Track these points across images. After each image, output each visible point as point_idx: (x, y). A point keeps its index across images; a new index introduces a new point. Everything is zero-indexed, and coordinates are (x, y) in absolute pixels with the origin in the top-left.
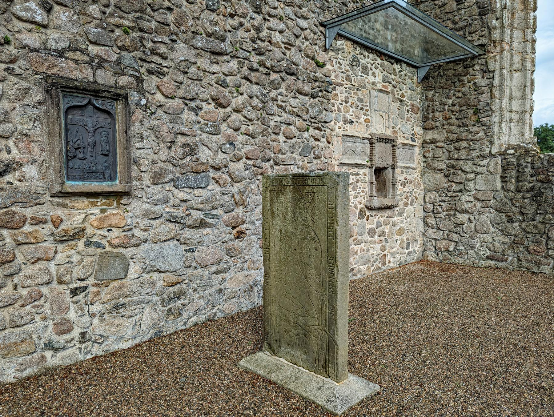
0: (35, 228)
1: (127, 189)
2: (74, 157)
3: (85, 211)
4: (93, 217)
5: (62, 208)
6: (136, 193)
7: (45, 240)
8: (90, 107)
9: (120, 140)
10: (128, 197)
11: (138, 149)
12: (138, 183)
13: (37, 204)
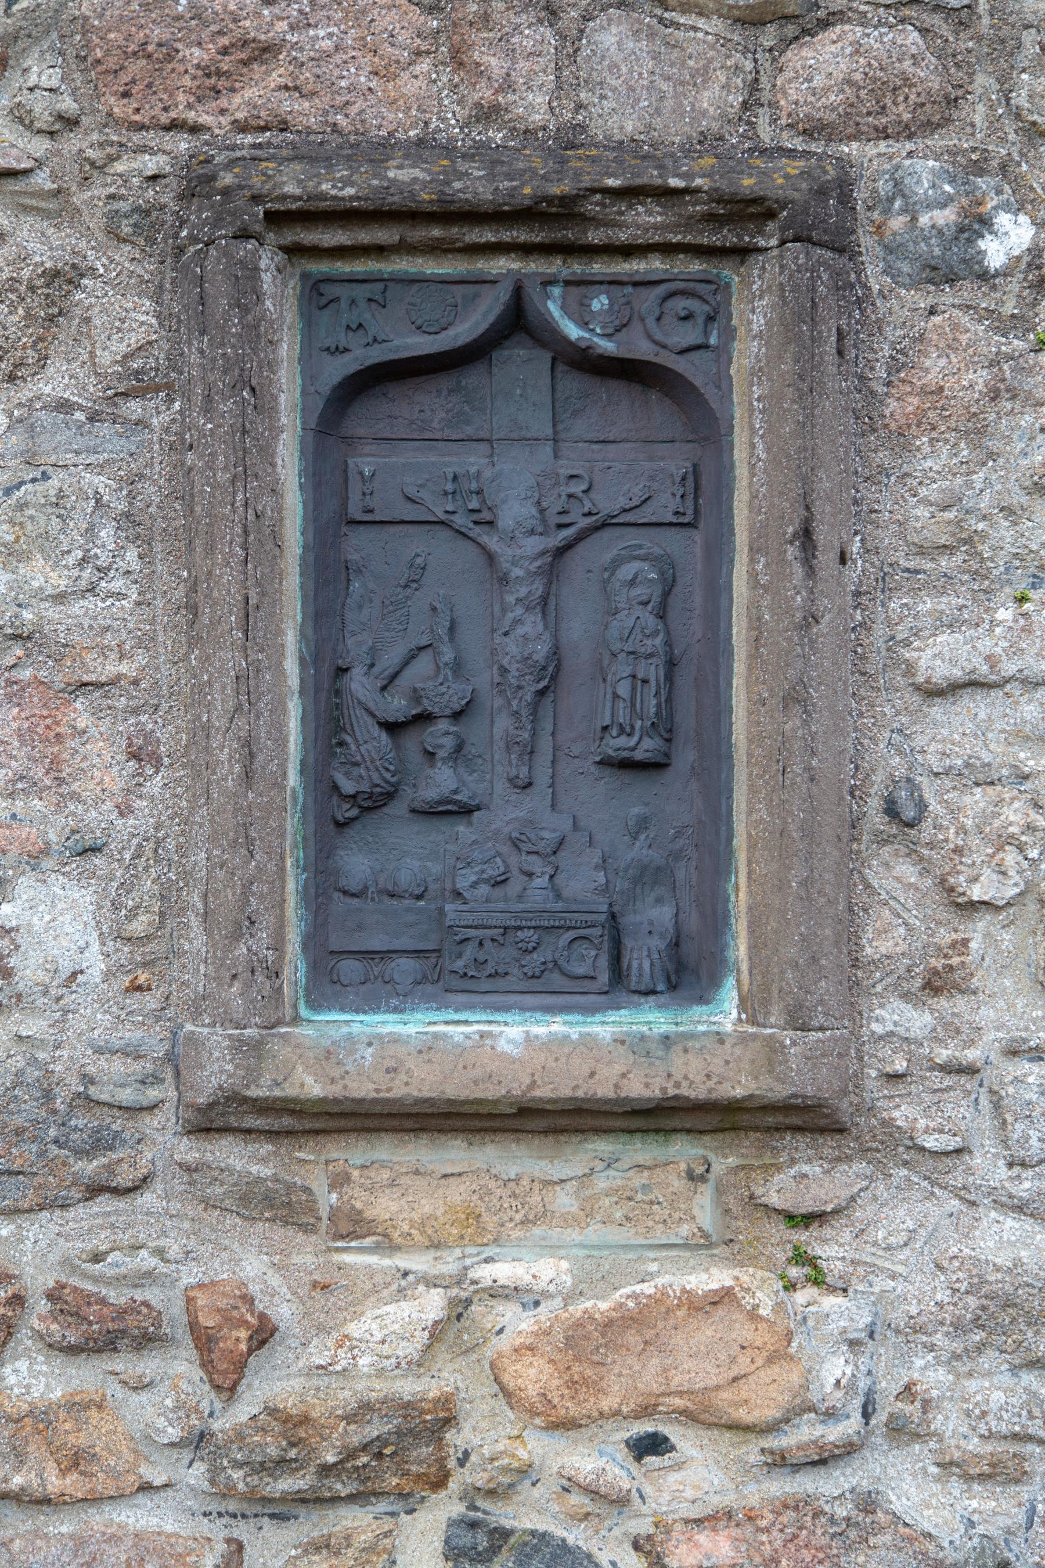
0: (86, 1376)
1: (798, 1078)
2: (374, 802)
3: (449, 1264)
4: (518, 1322)
5: (278, 1233)
6: (902, 1114)
7: (146, 1488)
8: (522, 367)
9: (756, 623)
10: (829, 1145)
11: (933, 692)
12: (918, 1021)
13: (94, 1190)
